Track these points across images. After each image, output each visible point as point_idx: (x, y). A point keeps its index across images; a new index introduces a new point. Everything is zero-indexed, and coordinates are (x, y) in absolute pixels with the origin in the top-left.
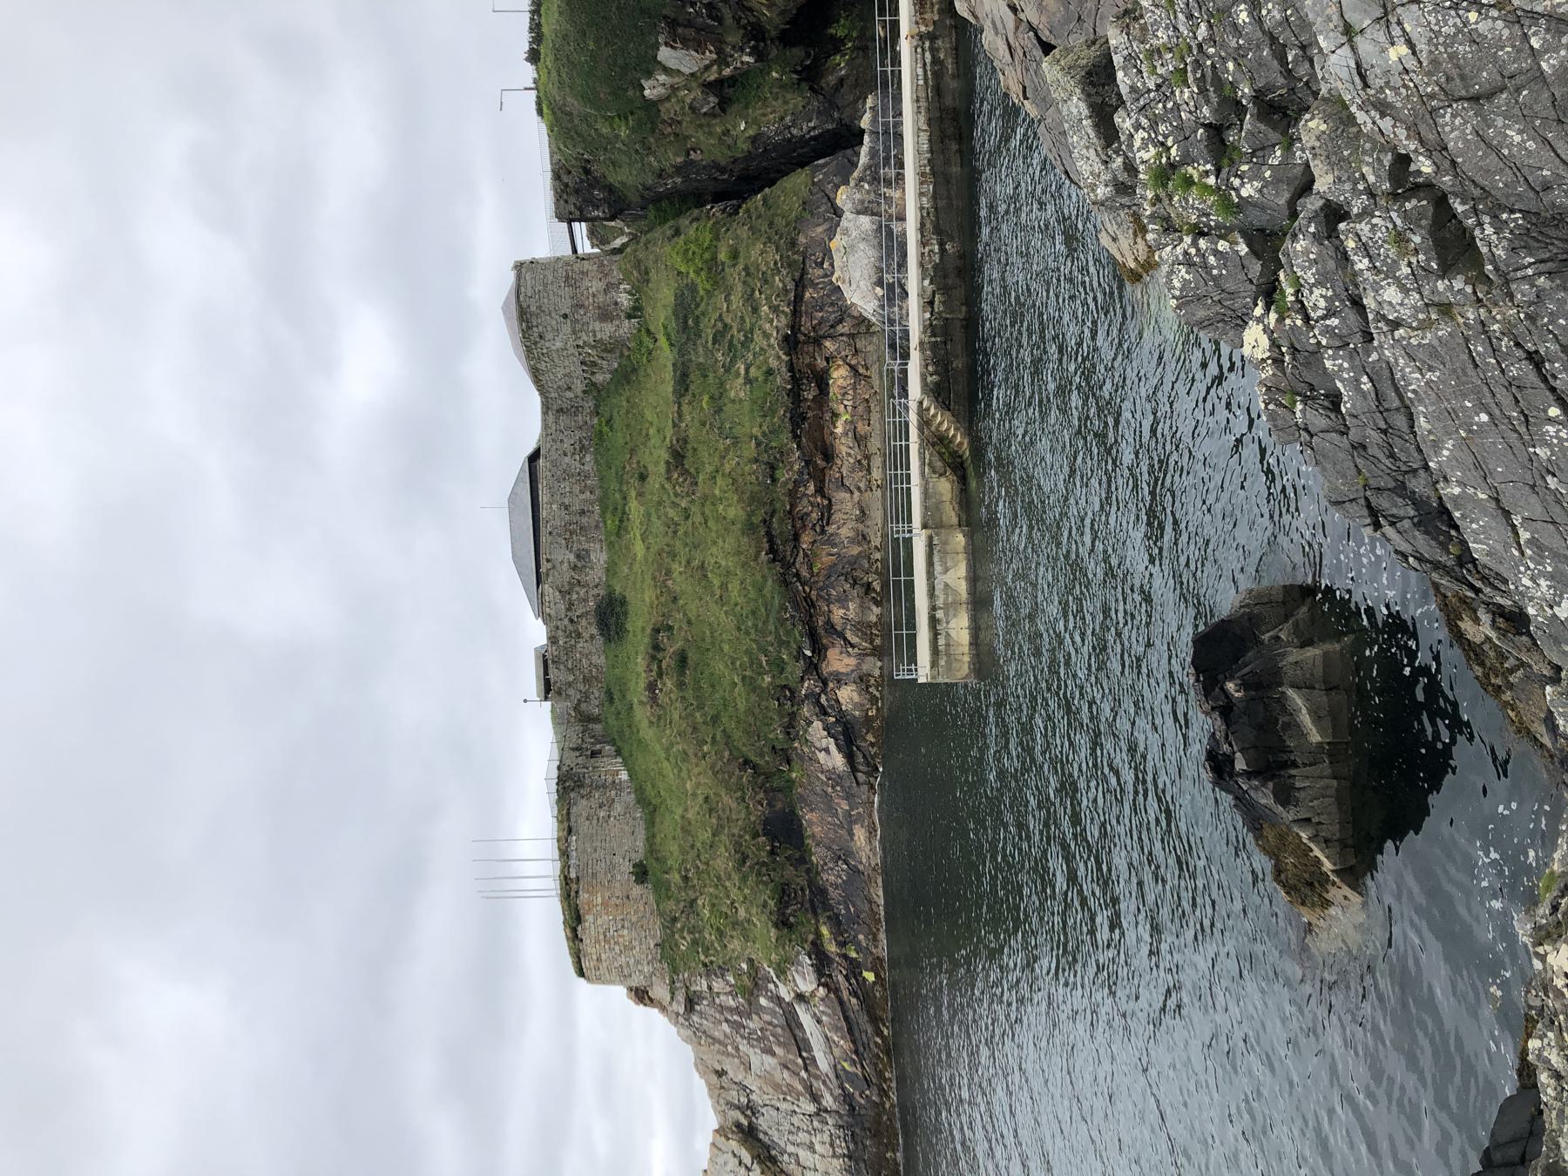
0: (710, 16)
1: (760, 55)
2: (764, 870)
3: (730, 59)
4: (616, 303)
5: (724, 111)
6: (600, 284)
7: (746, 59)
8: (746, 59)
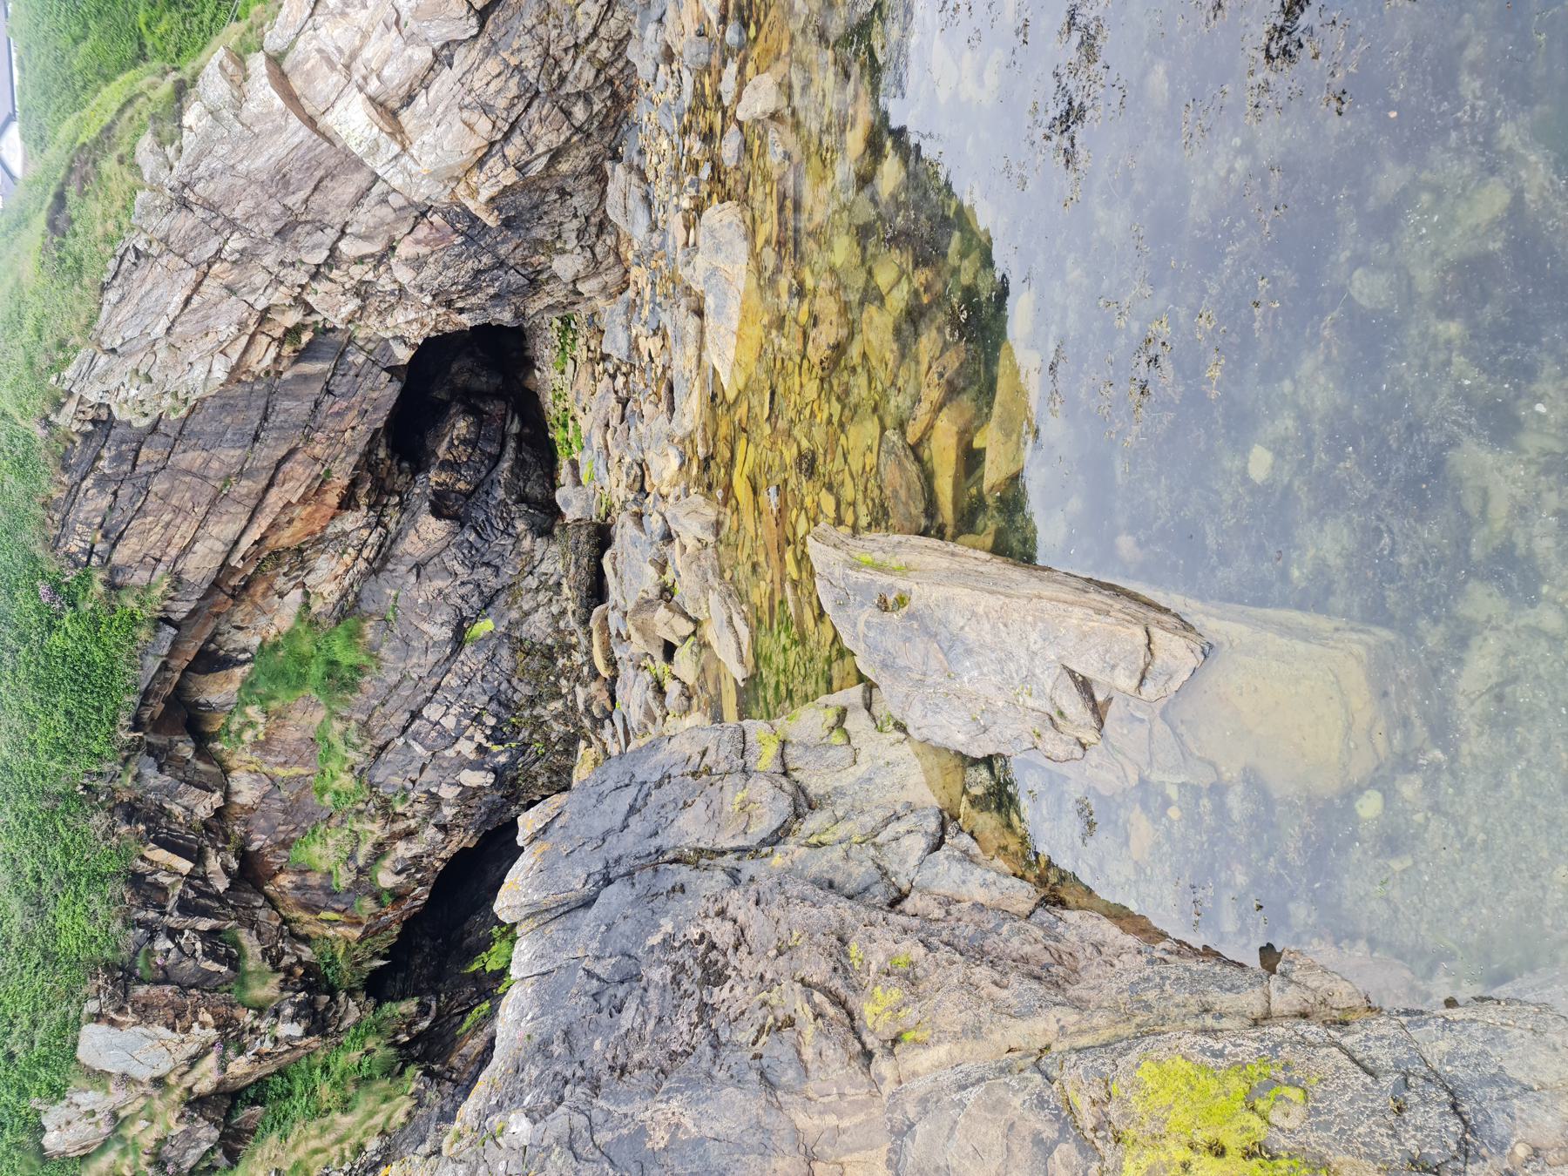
0: (210, 954)
1: (319, 1023)
2: (61, 806)
5: (233, 1158)
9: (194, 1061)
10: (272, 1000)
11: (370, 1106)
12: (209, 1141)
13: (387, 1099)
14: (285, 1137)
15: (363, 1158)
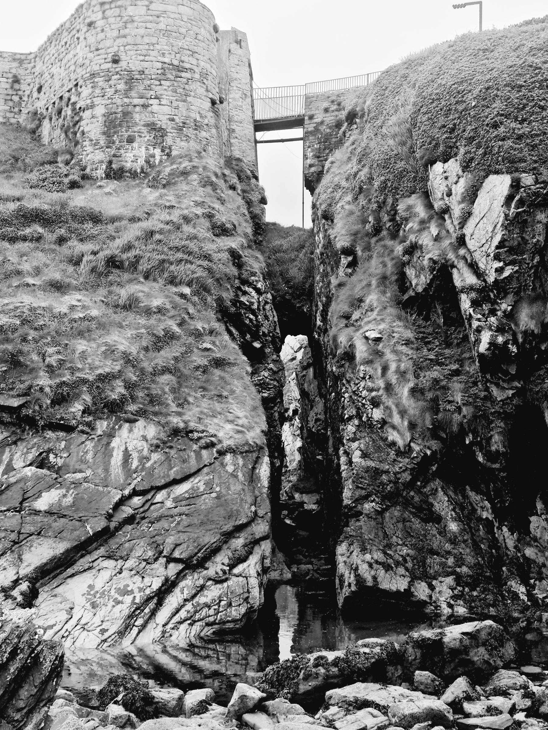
3: (486, 307)
4: (131, 140)
6: (164, 118)
7: (486, 337)
8: (486, 337)
9: (473, 267)
10: (517, 325)
11: (411, 412)
12: (417, 285)
13: (412, 426)
14: (408, 343)
15: (369, 407)
